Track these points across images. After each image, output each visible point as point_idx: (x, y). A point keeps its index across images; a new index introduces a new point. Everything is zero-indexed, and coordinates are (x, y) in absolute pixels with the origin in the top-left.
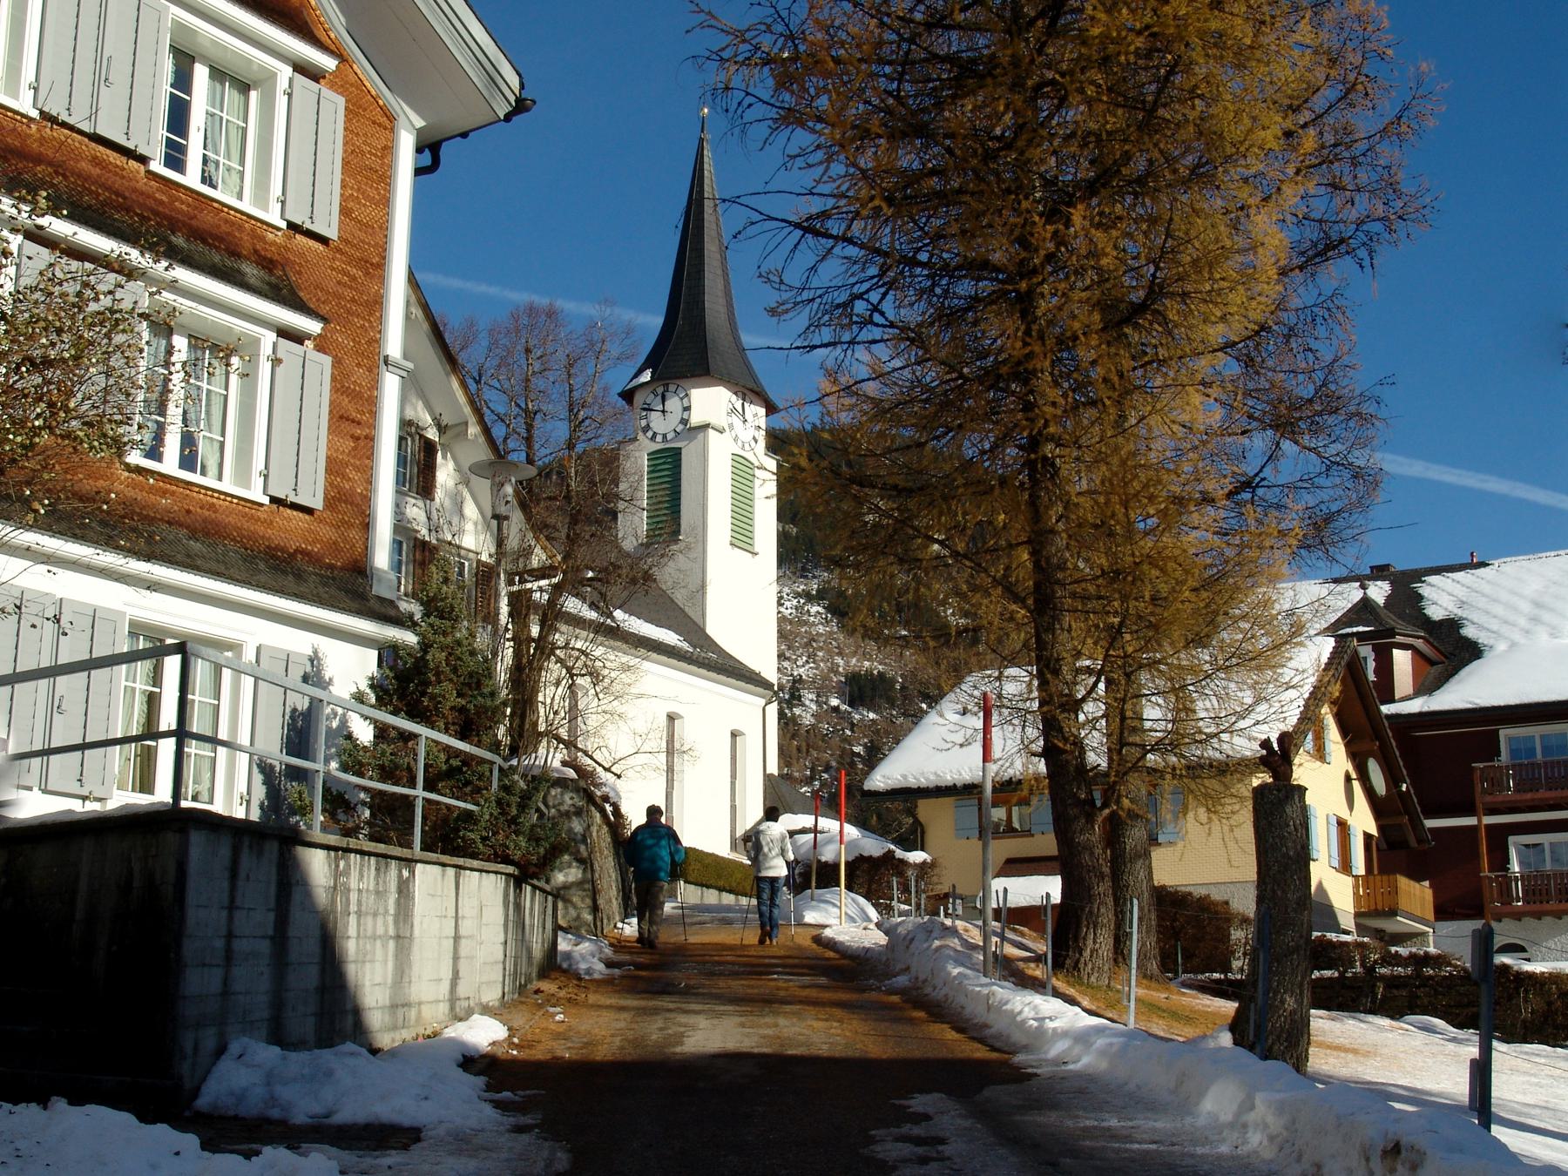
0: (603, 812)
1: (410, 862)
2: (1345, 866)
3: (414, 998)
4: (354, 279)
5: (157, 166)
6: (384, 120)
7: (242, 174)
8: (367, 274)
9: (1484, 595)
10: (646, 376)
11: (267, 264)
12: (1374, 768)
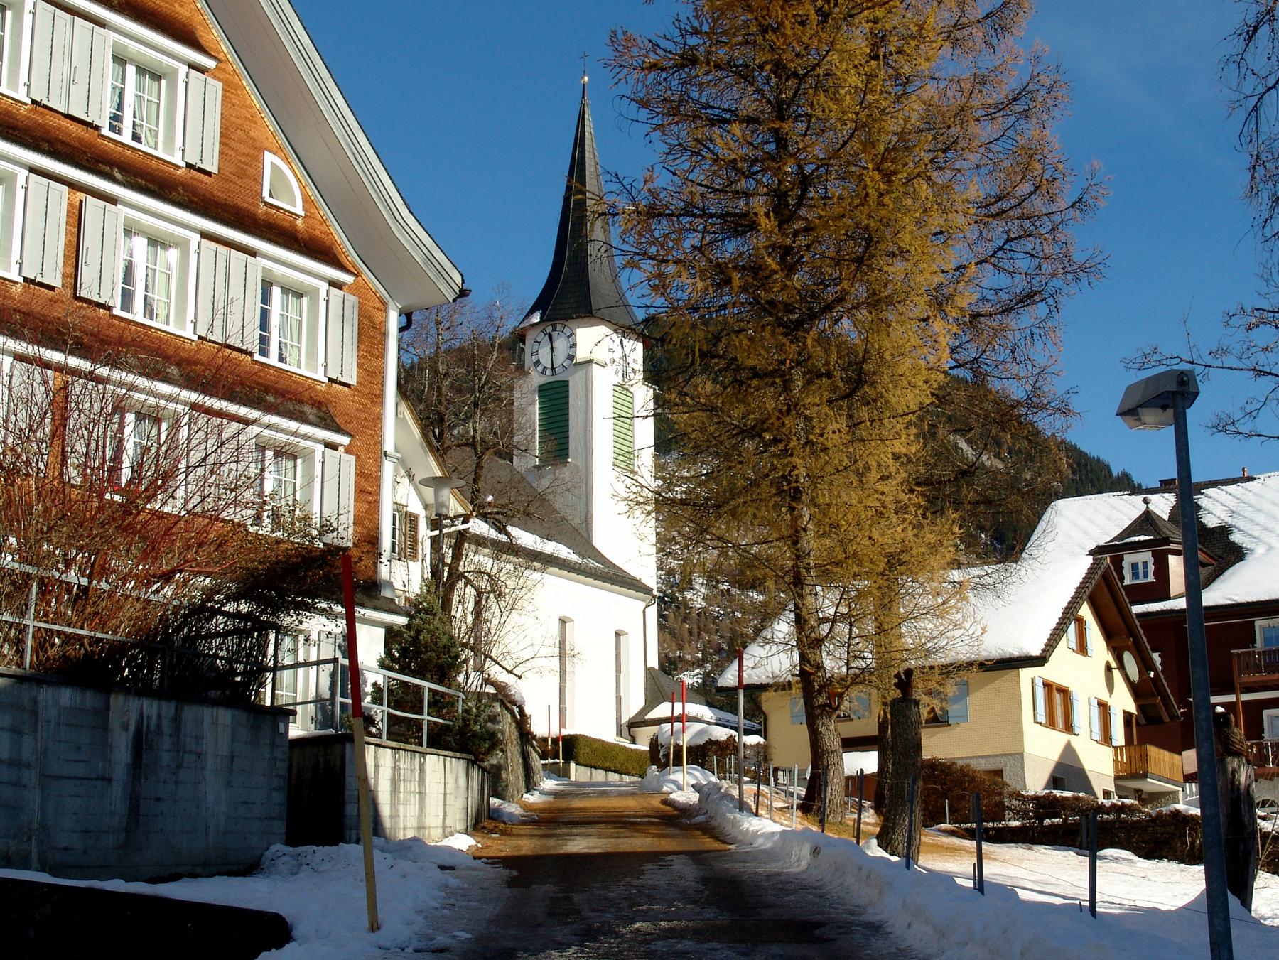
0: (512, 713)
1: (424, 754)
2: (1107, 739)
3: (427, 824)
4: (365, 406)
5: (257, 357)
6: (382, 307)
7: (299, 349)
8: (372, 402)
9: (1250, 506)
10: (536, 318)
11: (318, 404)
12: (1128, 658)
